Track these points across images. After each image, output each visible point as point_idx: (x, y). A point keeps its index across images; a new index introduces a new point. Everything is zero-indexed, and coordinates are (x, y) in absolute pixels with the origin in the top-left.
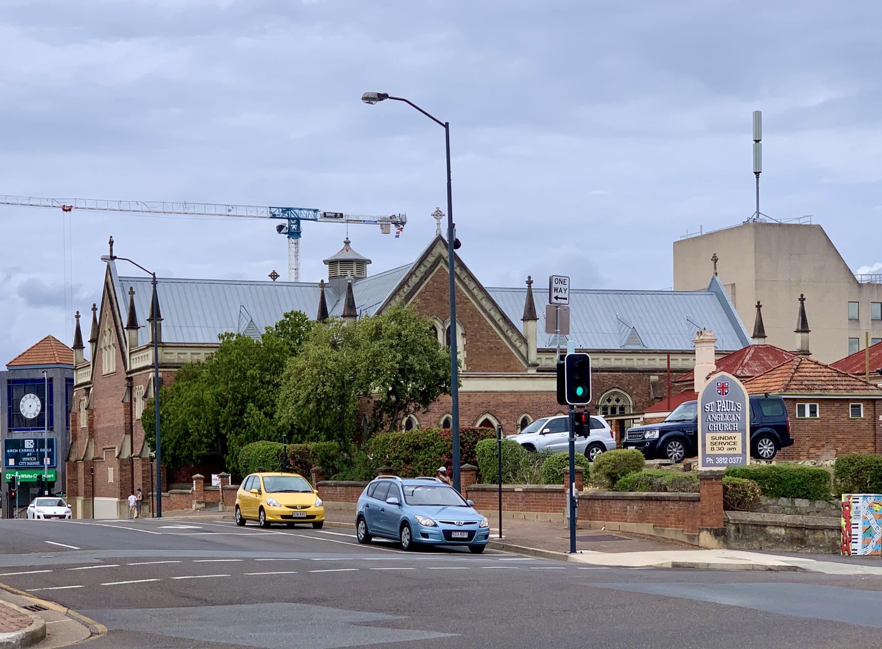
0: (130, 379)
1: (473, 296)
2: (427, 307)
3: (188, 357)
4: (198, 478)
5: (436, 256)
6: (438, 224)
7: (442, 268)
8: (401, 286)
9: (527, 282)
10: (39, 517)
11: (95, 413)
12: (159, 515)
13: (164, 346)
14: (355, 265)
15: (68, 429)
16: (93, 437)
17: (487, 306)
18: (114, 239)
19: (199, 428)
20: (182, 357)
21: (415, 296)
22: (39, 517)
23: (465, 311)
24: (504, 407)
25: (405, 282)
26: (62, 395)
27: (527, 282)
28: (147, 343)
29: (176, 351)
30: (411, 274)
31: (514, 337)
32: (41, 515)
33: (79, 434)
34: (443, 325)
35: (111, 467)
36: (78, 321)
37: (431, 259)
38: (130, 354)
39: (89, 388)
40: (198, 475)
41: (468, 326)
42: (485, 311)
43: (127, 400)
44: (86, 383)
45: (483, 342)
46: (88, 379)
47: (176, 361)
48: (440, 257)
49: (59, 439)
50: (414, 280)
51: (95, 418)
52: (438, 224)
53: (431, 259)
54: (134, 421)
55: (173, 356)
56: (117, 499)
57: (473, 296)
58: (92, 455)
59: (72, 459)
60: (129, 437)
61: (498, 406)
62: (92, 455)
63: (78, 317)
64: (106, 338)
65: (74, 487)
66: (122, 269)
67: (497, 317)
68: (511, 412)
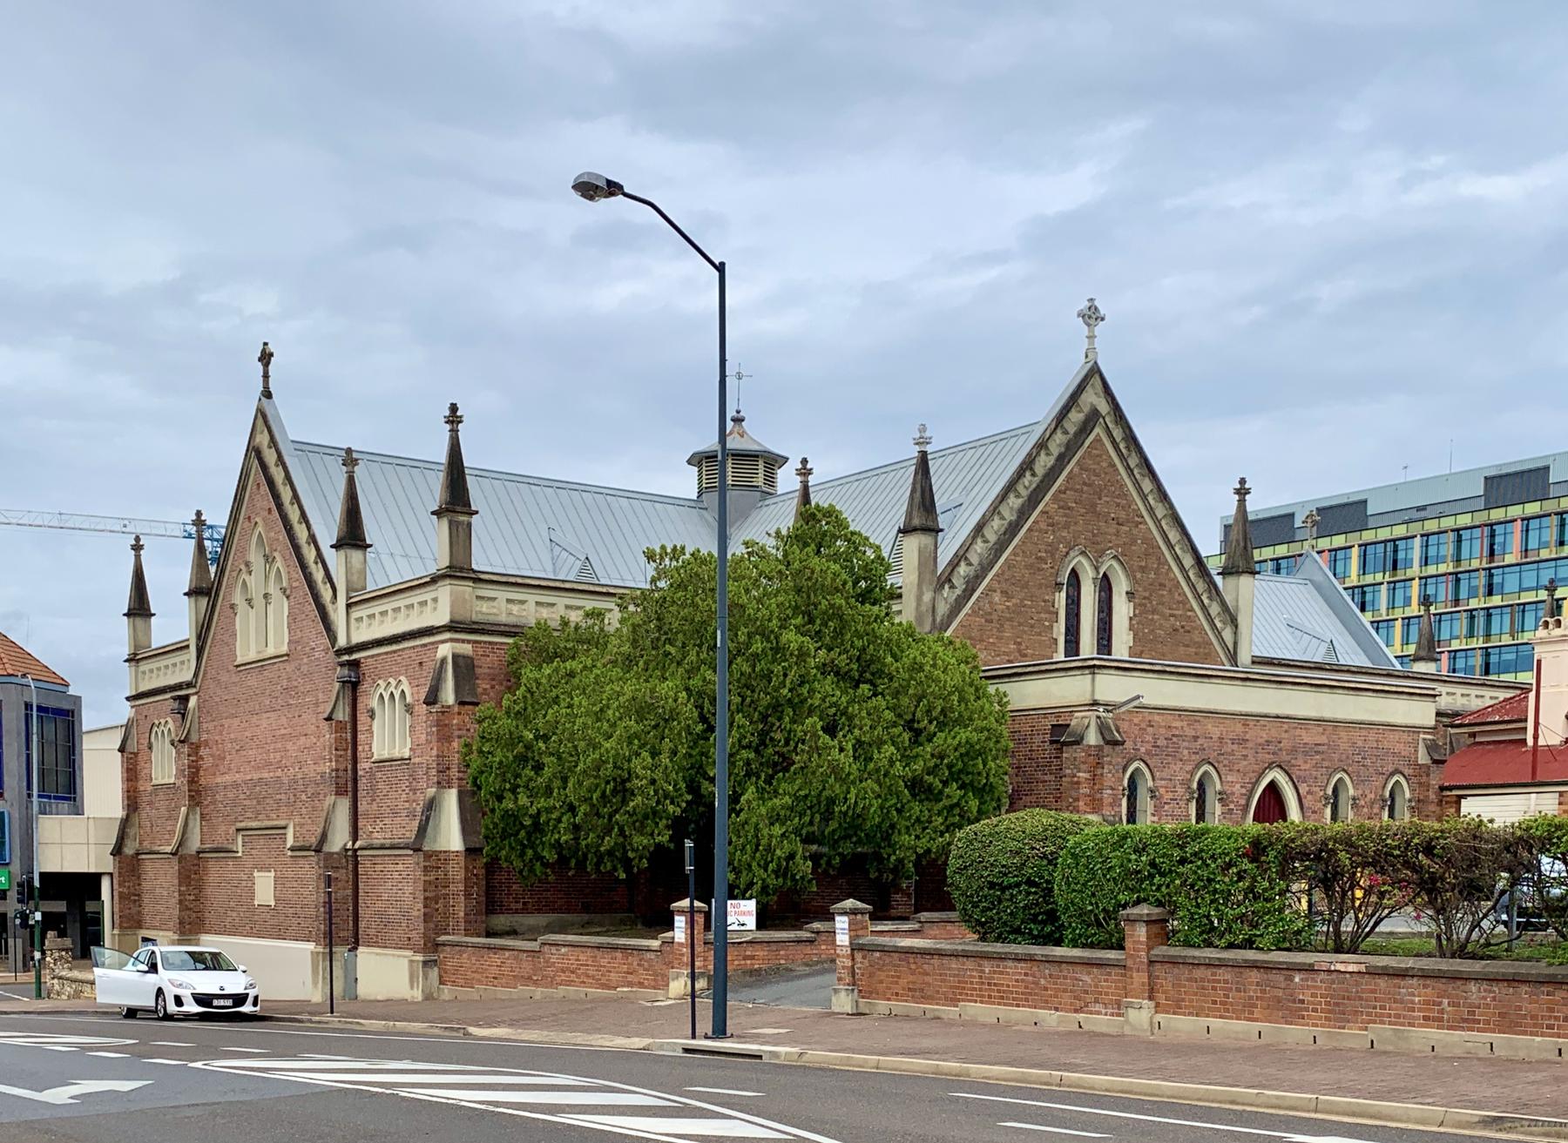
0: (355, 664)
1: (1151, 511)
2: (1066, 526)
3: (529, 610)
4: (853, 912)
5: (1086, 409)
6: (1091, 337)
7: (1098, 440)
8: (1020, 473)
9: (1238, 492)
10: (179, 1001)
11: (203, 752)
12: (720, 1031)
13: (477, 579)
14: (761, 464)
15: (30, 796)
16: (197, 804)
17: (1174, 536)
18: (271, 348)
19: (658, 775)
20: (515, 609)
21: (1047, 498)
22: (179, 1001)
23: (1134, 542)
24: (1306, 753)
25: (1027, 465)
26: (19, 734)
27: (1238, 492)
28: (432, 569)
29: (502, 594)
30: (1042, 445)
31: (1215, 609)
32: (186, 995)
33: (144, 800)
34: (1097, 569)
35: (264, 868)
36: (138, 557)
37: (1076, 417)
38: (349, 606)
39: (186, 699)
40: (850, 903)
41: (1139, 575)
42: (1170, 546)
43: (342, 714)
44: (179, 687)
45: (1162, 615)
46: (187, 676)
47: (503, 619)
48: (1094, 415)
49: (16, 815)
50: (1044, 463)
51: (207, 762)
52: (1091, 337)
53: (1076, 417)
54: (363, 765)
55: (499, 607)
56: (311, 946)
57: (1151, 511)
58: (194, 844)
59: (129, 850)
60: (344, 805)
61: (1293, 751)
62: (194, 844)
63: (137, 547)
64: (254, 582)
65: (135, 910)
66: (294, 425)
67: (1188, 561)
68: (1315, 766)
